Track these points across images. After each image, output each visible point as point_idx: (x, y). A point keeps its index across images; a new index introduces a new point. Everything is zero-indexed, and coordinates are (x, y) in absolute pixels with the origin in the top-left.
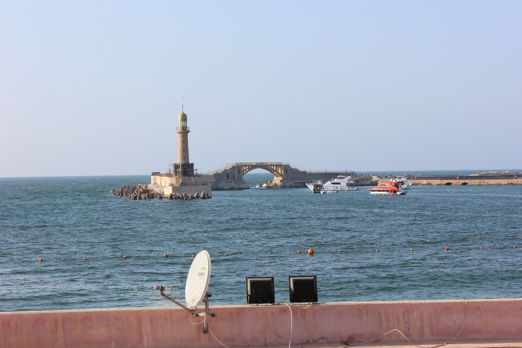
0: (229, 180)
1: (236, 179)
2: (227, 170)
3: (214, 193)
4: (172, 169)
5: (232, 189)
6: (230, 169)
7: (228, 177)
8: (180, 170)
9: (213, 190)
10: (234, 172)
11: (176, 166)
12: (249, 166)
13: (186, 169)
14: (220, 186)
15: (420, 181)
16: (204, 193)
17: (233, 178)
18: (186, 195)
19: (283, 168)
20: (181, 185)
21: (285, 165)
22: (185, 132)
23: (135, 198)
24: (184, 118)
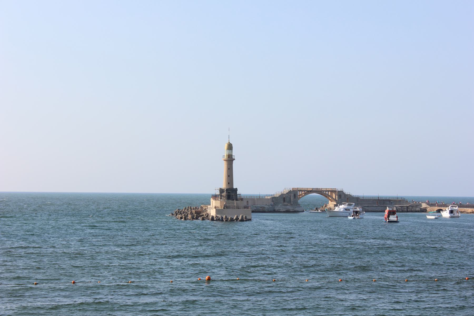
0: (285, 203)
1: (292, 203)
2: (284, 194)
3: (254, 216)
4: (218, 193)
5: (288, 212)
6: (287, 193)
7: (284, 201)
8: (224, 194)
9: (253, 212)
10: (291, 197)
11: (221, 191)
12: (304, 191)
13: (230, 194)
14: (277, 208)
15: (465, 209)
16: (242, 216)
17: (289, 202)
18: (226, 217)
19: (337, 193)
20: (224, 208)
21: (339, 191)
22: (230, 160)
23: (181, 218)
24: (230, 147)
